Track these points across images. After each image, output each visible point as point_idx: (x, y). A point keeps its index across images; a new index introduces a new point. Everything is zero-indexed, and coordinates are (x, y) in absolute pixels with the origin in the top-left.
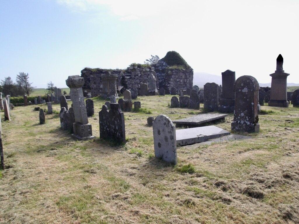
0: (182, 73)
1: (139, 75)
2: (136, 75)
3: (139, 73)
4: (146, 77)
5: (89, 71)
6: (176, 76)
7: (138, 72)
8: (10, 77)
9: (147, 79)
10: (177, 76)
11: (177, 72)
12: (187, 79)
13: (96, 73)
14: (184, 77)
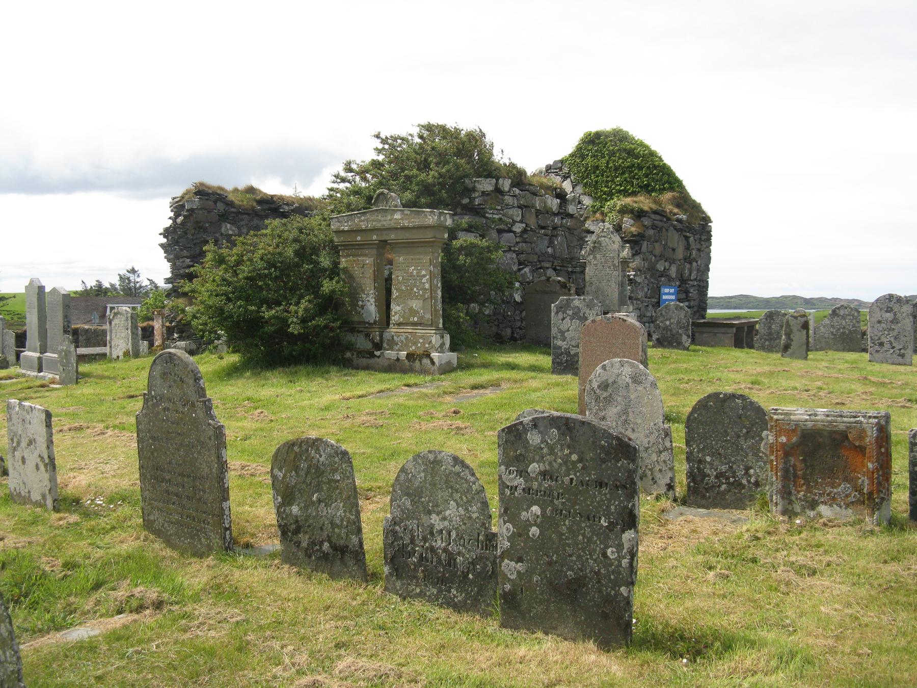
0: (675, 232)
1: (518, 228)
2: (502, 227)
3: (517, 214)
4: (546, 243)
5: (215, 202)
6: (657, 245)
7: (511, 212)
8: (162, 231)
9: (550, 250)
10: (658, 249)
11: (660, 224)
12: (690, 263)
13: (248, 214)
14: (680, 253)
